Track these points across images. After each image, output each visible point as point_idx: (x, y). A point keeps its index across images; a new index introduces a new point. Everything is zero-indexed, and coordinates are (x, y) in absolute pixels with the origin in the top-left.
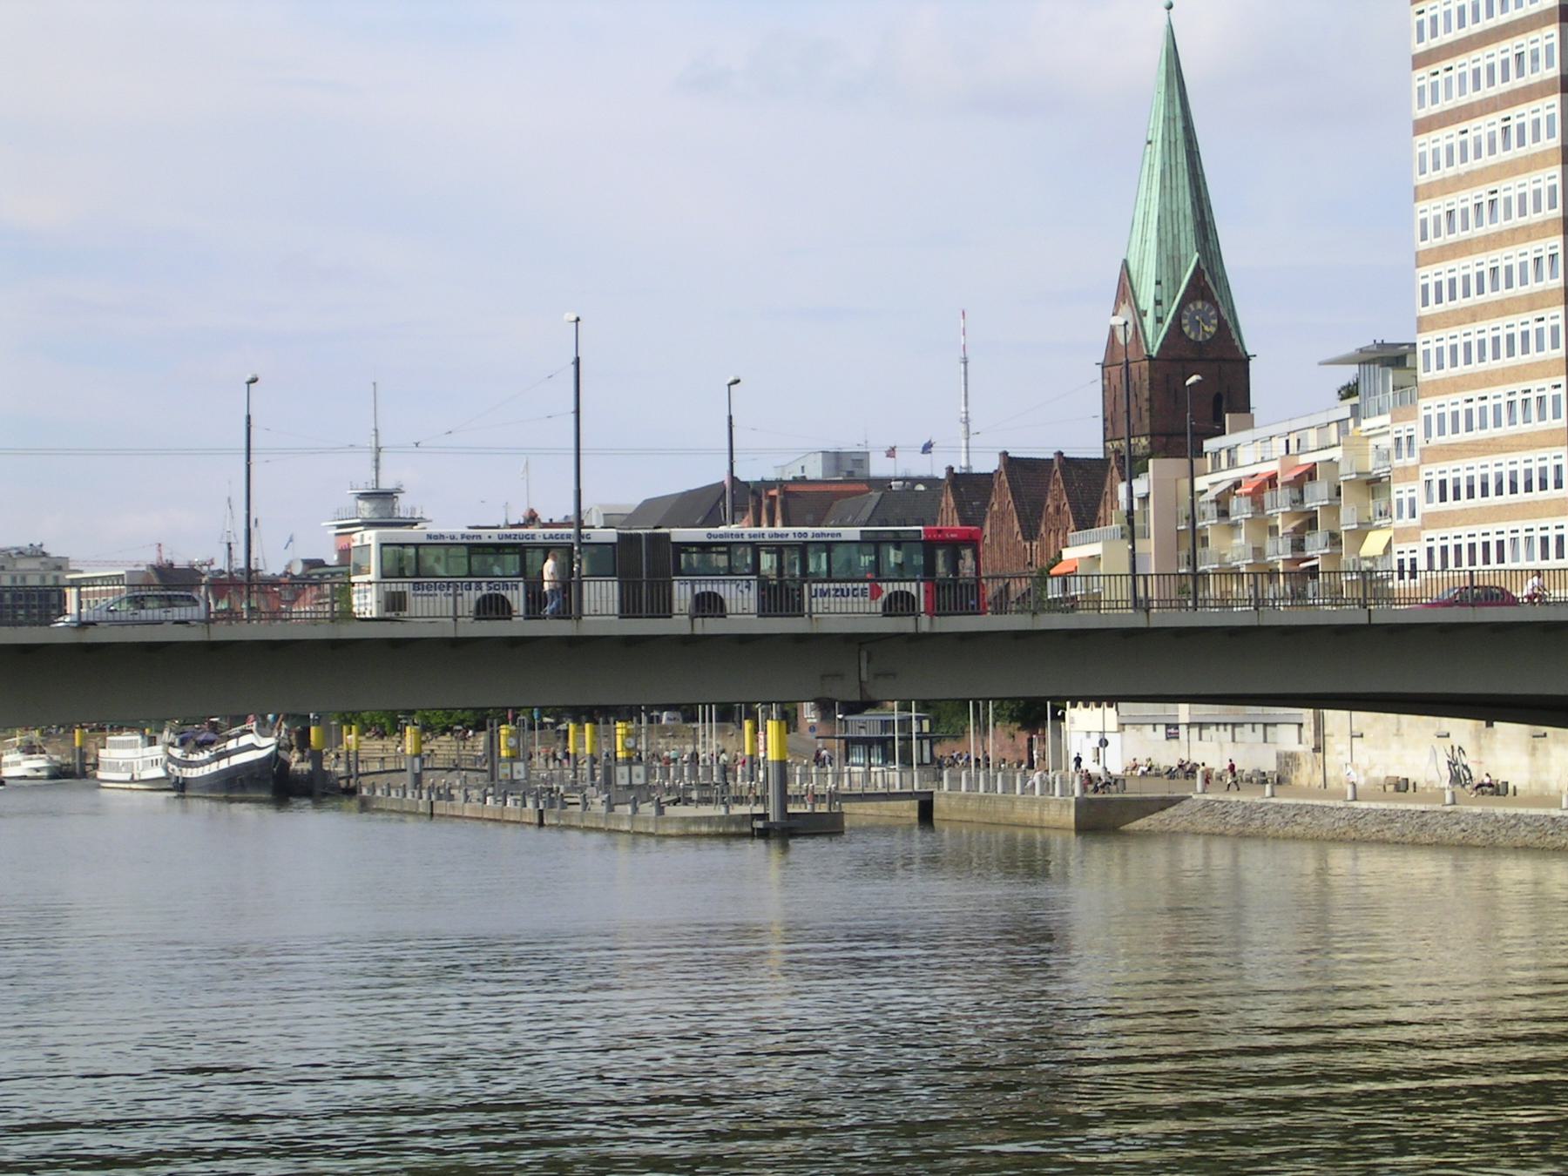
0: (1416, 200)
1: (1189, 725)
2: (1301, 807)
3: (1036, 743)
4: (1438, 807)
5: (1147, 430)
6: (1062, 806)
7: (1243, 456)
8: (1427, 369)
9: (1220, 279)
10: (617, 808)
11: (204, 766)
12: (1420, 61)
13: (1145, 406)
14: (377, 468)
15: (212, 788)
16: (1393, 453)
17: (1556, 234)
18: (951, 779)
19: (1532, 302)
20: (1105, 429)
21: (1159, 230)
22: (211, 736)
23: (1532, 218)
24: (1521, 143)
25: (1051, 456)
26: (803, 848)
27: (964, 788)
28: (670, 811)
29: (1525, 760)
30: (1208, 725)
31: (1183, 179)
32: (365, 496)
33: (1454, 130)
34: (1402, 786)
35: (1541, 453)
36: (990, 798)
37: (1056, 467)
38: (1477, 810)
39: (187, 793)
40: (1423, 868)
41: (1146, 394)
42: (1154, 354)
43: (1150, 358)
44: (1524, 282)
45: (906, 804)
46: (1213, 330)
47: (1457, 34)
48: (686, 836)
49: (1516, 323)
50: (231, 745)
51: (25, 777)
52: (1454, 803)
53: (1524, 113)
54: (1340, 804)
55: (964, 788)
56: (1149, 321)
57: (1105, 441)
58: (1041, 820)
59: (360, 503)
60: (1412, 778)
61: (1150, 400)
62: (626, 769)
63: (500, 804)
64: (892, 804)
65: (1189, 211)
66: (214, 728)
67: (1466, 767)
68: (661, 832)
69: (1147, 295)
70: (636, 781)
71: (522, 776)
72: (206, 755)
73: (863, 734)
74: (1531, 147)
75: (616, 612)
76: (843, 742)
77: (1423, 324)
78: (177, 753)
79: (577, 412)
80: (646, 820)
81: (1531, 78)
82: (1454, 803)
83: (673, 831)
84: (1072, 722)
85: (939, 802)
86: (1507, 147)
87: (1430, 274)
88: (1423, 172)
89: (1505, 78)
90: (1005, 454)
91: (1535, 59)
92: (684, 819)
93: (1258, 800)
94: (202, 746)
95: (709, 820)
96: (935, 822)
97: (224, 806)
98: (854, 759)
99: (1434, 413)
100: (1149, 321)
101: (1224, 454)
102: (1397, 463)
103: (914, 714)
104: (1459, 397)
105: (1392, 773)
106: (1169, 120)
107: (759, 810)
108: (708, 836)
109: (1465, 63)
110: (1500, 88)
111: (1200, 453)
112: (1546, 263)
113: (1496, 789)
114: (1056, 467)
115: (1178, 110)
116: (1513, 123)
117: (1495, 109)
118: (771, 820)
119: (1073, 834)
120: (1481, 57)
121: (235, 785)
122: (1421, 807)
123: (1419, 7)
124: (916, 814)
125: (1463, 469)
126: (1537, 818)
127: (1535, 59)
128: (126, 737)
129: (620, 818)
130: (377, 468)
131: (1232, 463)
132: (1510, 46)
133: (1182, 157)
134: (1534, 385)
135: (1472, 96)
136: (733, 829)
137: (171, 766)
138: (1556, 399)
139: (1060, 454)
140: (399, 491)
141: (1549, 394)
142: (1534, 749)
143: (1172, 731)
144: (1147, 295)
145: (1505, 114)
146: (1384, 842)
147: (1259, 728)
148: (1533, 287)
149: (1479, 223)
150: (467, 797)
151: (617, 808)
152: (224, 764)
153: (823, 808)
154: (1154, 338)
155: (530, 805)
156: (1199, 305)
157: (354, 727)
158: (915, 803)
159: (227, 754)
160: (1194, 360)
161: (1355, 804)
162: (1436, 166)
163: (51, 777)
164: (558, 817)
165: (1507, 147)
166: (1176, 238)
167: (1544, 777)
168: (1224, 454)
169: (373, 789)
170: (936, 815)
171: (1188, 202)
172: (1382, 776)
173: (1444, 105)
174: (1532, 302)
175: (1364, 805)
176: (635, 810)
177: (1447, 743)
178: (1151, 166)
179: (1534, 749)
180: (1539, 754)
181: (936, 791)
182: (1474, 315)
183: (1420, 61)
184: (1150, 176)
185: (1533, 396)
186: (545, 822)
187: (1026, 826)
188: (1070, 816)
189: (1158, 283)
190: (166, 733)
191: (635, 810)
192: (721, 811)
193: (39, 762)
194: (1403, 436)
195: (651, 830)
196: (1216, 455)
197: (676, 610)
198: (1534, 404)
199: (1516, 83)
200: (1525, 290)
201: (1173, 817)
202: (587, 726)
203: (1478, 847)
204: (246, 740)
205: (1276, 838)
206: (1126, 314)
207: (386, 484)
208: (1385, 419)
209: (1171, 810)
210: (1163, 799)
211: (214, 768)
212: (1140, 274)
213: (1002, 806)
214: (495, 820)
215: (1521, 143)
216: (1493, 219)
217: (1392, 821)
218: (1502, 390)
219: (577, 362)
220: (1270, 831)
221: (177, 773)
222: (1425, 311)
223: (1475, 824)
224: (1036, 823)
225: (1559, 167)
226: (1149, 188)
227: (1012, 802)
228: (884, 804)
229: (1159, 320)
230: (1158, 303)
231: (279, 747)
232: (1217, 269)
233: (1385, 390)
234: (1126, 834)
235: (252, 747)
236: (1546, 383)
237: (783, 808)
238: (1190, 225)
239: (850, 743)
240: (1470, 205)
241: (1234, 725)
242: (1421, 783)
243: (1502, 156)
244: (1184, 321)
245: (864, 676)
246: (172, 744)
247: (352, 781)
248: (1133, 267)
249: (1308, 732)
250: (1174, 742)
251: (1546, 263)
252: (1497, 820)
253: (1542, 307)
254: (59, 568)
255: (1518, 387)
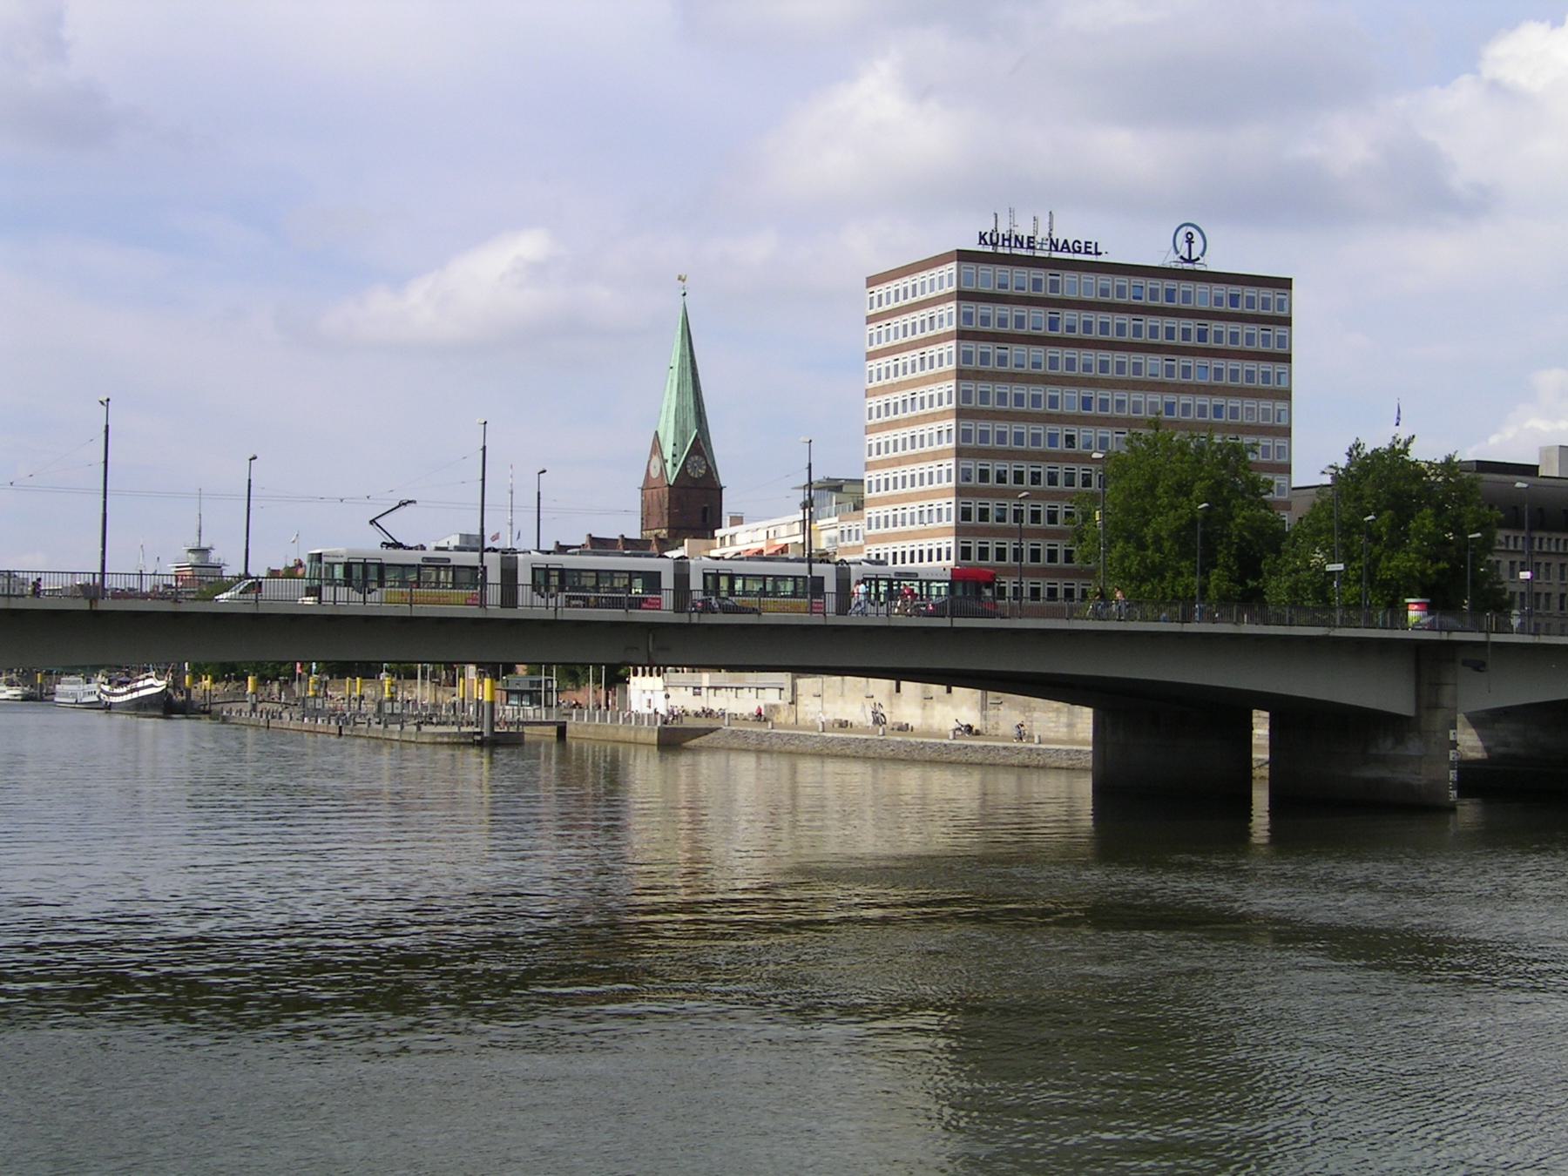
0: (866, 396)
1: (708, 688)
2: (792, 735)
3: (610, 696)
4: (875, 737)
5: (666, 525)
6: (649, 731)
7: (739, 539)
8: (870, 492)
9: (708, 443)
10: (390, 726)
11: (122, 696)
12: (870, 320)
13: (666, 511)
14: (200, 536)
15: (128, 709)
16: (839, 540)
17: (951, 418)
18: (577, 714)
19: (935, 456)
20: (642, 524)
21: (676, 416)
22: (128, 679)
23: (936, 408)
24: (931, 367)
25: (617, 537)
26: (502, 755)
27: (586, 719)
28: (424, 728)
29: (919, 712)
30: (720, 688)
31: (689, 389)
32: (190, 551)
33: (891, 358)
34: (844, 725)
35: (939, 540)
36: (604, 726)
37: (620, 543)
38: (899, 739)
39: (112, 711)
40: (857, 775)
41: (666, 506)
42: (671, 483)
43: (669, 485)
44: (931, 444)
45: (549, 728)
46: (703, 472)
47: (893, 305)
48: (435, 743)
49: (925, 467)
50: (140, 684)
51: (8, 699)
52: (884, 735)
53: (933, 350)
54: (815, 734)
55: (586, 719)
56: (669, 466)
57: (642, 530)
58: (635, 739)
59: (190, 554)
60: (850, 719)
61: (669, 508)
62: (390, 704)
63: (313, 722)
64: (540, 728)
65: (692, 406)
66: (128, 674)
67: (882, 715)
68: (419, 740)
69: (668, 451)
70: (395, 711)
71: (321, 707)
72: (124, 689)
73: (518, 688)
74: (937, 369)
75: (499, 603)
76: (505, 693)
77: (869, 466)
78: (107, 688)
79: (483, 480)
80: (411, 734)
81: (938, 331)
82: (884, 735)
83: (427, 740)
84: (634, 684)
85: (568, 728)
86: (922, 369)
87: (874, 439)
88: (870, 382)
89: (923, 331)
90: (590, 535)
91: (941, 320)
92: (434, 733)
93: (765, 730)
94: (121, 684)
95: (448, 734)
96: (568, 739)
97: (135, 718)
98: (511, 702)
99: (874, 516)
100: (669, 466)
101: (728, 538)
102: (841, 544)
103: (543, 678)
104: (890, 508)
105: (838, 717)
106: (682, 356)
107: (478, 730)
108: (447, 743)
109: (898, 321)
110: (919, 335)
111: (713, 538)
112: (945, 434)
113: (904, 728)
114: (620, 543)
115: (688, 351)
116: (927, 356)
117: (916, 348)
118: (485, 735)
119: (656, 748)
120: (908, 318)
121: (141, 707)
122: (865, 737)
123: (871, 289)
124: (555, 734)
125: (890, 547)
126: (935, 744)
127: (941, 320)
128: (72, 678)
129: (392, 732)
130: (200, 536)
131: (732, 543)
132: (926, 313)
133: (689, 377)
134: (935, 502)
135: (902, 340)
136: (463, 740)
137: (102, 695)
138: (949, 510)
139: (622, 536)
140: (211, 548)
141: (944, 507)
142: (925, 705)
143: (697, 691)
144: (668, 451)
145: (922, 350)
146: (846, 757)
147: (754, 691)
148: (936, 447)
149: (905, 411)
150: (291, 718)
151: (390, 726)
152: (135, 695)
153: (512, 729)
154: (672, 475)
155: (333, 723)
156: (697, 458)
157: (209, 677)
158: (555, 727)
159: (137, 690)
160: (691, 488)
161: (824, 734)
162: (879, 379)
163: (22, 700)
164: (352, 731)
165: (922, 369)
166: (685, 420)
167: (930, 721)
168: (728, 538)
169: (230, 711)
170: (567, 735)
171: (692, 401)
172: (832, 719)
173: (884, 344)
174: (935, 456)
175: (830, 735)
176: (402, 728)
177: (872, 701)
178: (672, 381)
179: (925, 705)
180: (927, 708)
181: (568, 721)
182: (899, 462)
183: (870, 320)
184: (671, 386)
185: (935, 508)
186: (343, 733)
187: (625, 742)
188: (654, 737)
189: (675, 445)
190: (100, 676)
191: (402, 728)
192: (455, 729)
193: (16, 691)
194: (846, 529)
195: (413, 739)
196: (722, 538)
197: (520, 603)
198: (935, 513)
199: (929, 333)
200: (931, 449)
201: (713, 739)
202: (358, 679)
203: (903, 760)
204: (148, 682)
205: (780, 752)
206: (656, 461)
207: (204, 545)
208: (835, 520)
209: (712, 735)
210: (707, 729)
211: (129, 697)
212: (664, 439)
213: (611, 731)
214: (310, 731)
215: (931, 367)
216: (913, 409)
217: (849, 744)
218: (916, 504)
219: (484, 449)
220: (776, 748)
221: (107, 700)
222: (870, 459)
223: (899, 748)
224: (632, 740)
225: (954, 381)
226: (671, 393)
227: (617, 729)
228: (535, 728)
229: (675, 465)
230: (674, 455)
231: (167, 686)
232: (706, 438)
233: (831, 504)
234: (685, 748)
235: (152, 686)
236: (943, 501)
237: (492, 728)
238: (693, 414)
239: (510, 692)
240: (899, 401)
241: (737, 688)
242: (855, 723)
243: (919, 373)
244: (688, 466)
245: (651, 650)
246: (104, 683)
247: (207, 707)
248: (661, 435)
249: (787, 694)
250: (698, 697)
251: (945, 434)
252: (912, 745)
253: (942, 458)
254: (23, 584)
255: (926, 503)
